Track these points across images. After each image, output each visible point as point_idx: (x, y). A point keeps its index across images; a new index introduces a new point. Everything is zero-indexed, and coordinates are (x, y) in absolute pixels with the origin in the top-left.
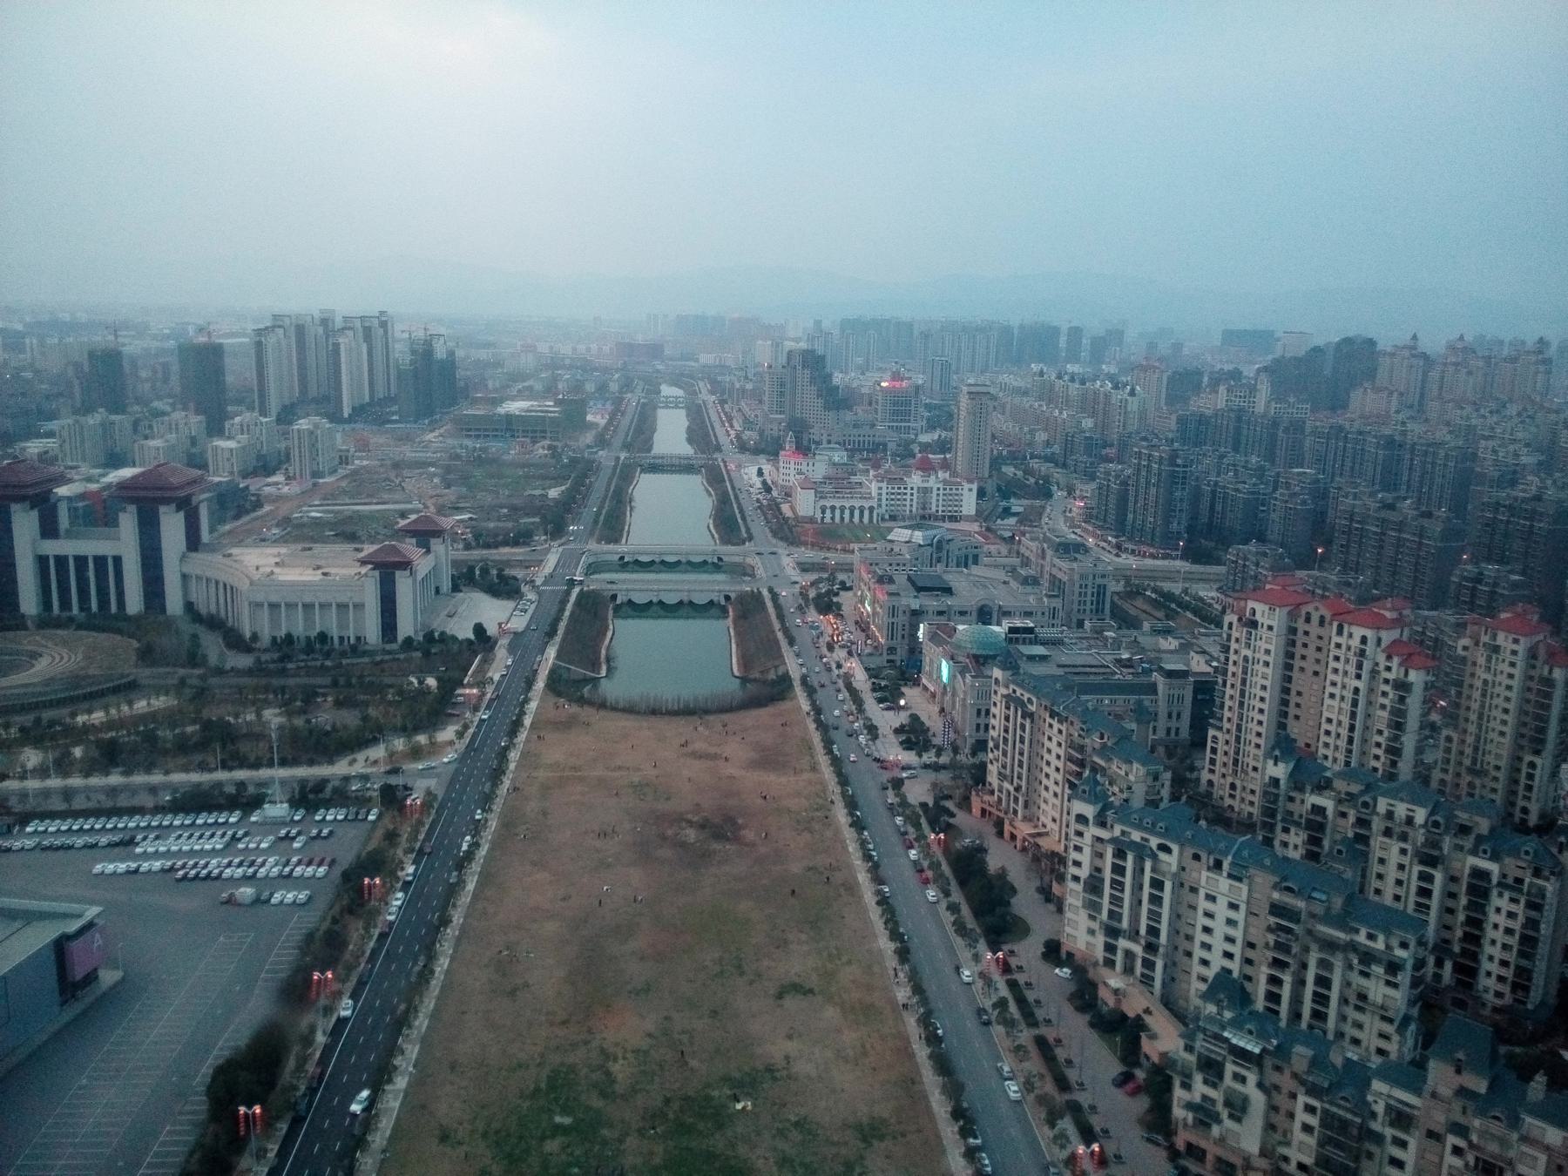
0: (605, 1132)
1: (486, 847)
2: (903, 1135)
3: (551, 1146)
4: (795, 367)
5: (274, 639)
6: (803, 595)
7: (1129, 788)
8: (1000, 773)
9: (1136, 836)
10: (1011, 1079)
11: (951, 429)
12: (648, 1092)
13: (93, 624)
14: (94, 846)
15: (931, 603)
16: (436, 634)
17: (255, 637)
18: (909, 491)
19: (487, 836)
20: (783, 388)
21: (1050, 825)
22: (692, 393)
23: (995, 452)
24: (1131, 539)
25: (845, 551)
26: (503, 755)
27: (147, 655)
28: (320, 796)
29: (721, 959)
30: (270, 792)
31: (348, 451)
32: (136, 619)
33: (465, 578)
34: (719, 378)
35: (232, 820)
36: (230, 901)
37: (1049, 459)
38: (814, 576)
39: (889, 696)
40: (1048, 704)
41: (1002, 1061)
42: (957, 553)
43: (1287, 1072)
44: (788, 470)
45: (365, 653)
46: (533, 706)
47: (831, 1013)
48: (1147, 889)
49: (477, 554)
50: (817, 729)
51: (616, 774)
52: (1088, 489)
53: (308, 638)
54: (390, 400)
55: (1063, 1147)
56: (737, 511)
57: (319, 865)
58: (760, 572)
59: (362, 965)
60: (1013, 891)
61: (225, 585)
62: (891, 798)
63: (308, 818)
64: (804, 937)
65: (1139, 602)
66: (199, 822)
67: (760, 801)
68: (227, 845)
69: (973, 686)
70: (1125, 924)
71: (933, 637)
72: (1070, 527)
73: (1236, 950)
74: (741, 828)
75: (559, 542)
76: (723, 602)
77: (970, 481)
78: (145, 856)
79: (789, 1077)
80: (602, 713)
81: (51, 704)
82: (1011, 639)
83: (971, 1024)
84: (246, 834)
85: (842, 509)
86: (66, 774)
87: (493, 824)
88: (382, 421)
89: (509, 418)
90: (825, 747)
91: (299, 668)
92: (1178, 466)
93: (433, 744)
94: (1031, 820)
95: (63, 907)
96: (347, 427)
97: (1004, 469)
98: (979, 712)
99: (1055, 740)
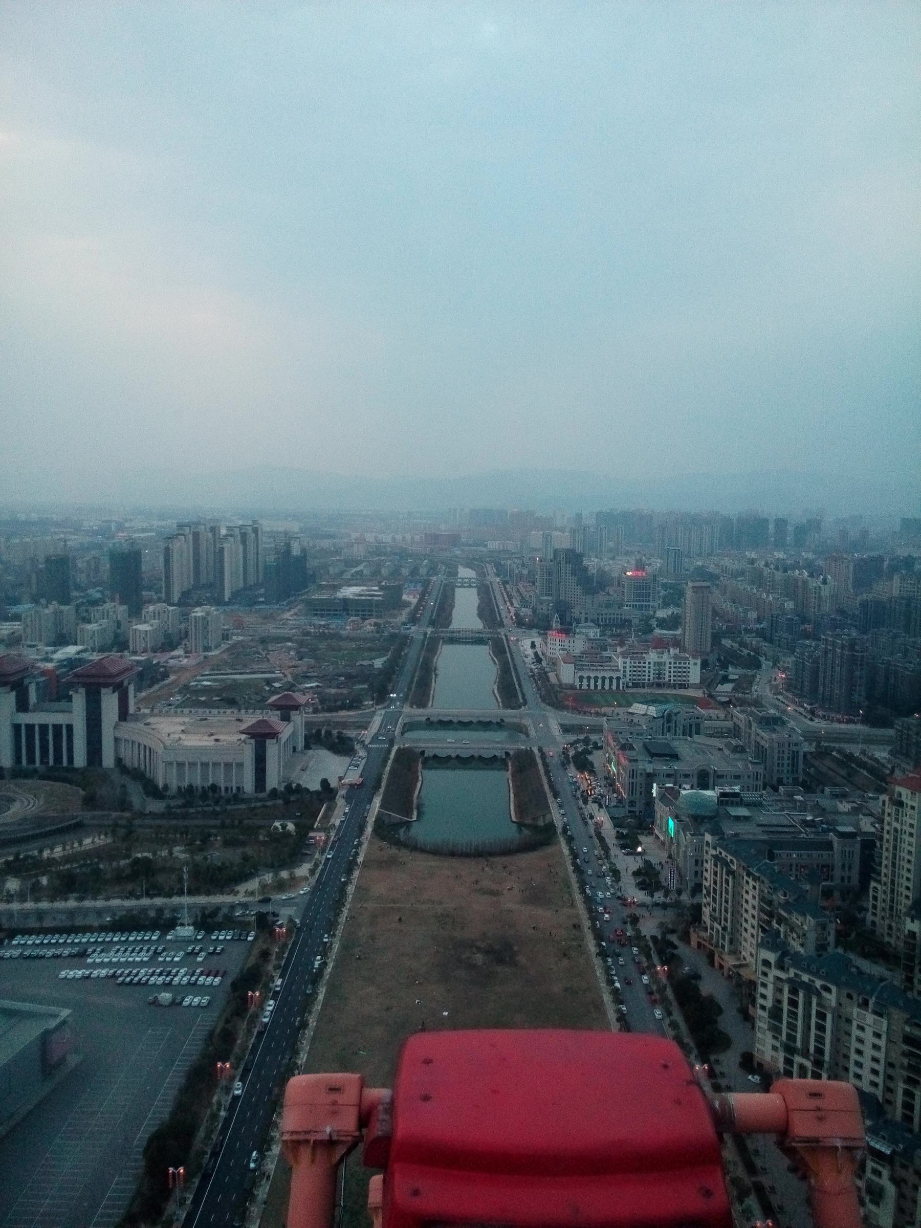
1: (331, 965)
5: (179, 788)
6: (565, 752)
7: (804, 935)
8: (711, 915)
9: (805, 978)
16: (294, 785)
17: (166, 787)
18: (647, 665)
21: (749, 959)
22: (482, 574)
24: (822, 707)
27: (90, 802)
32: (82, 772)
35: (154, 938)
36: (155, 1003)
37: (761, 634)
38: (572, 738)
40: (745, 865)
42: (683, 722)
43: (911, 1170)
45: (243, 801)
48: (814, 1020)
50: (574, 872)
51: (423, 907)
52: (789, 661)
53: (203, 788)
56: (515, 678)
57: (215, 976)
58: (532, 732)
60: (720, 1011)
61: (145, 747)
65: (828, 762)
67: (531, 931)
68: (151, 958)
70: (799, 1044)
71: (662, 797)
72: (775, 694)
73: (880, 1068)
77: (694, 657)
78: (95, 966)
80: (418, 855)
82: (722, 801)
84: (164, 950)
85: (596, 678)
86: (37, 900)
87: (336, 946)
88: (252, 603)
89: (345, 601)
92: (857, 651)
93: (293, 878)
95: (43, 1009)
96: (228, 608)
97: (724, 642)
98: (697, 862)
99: (751, 893)
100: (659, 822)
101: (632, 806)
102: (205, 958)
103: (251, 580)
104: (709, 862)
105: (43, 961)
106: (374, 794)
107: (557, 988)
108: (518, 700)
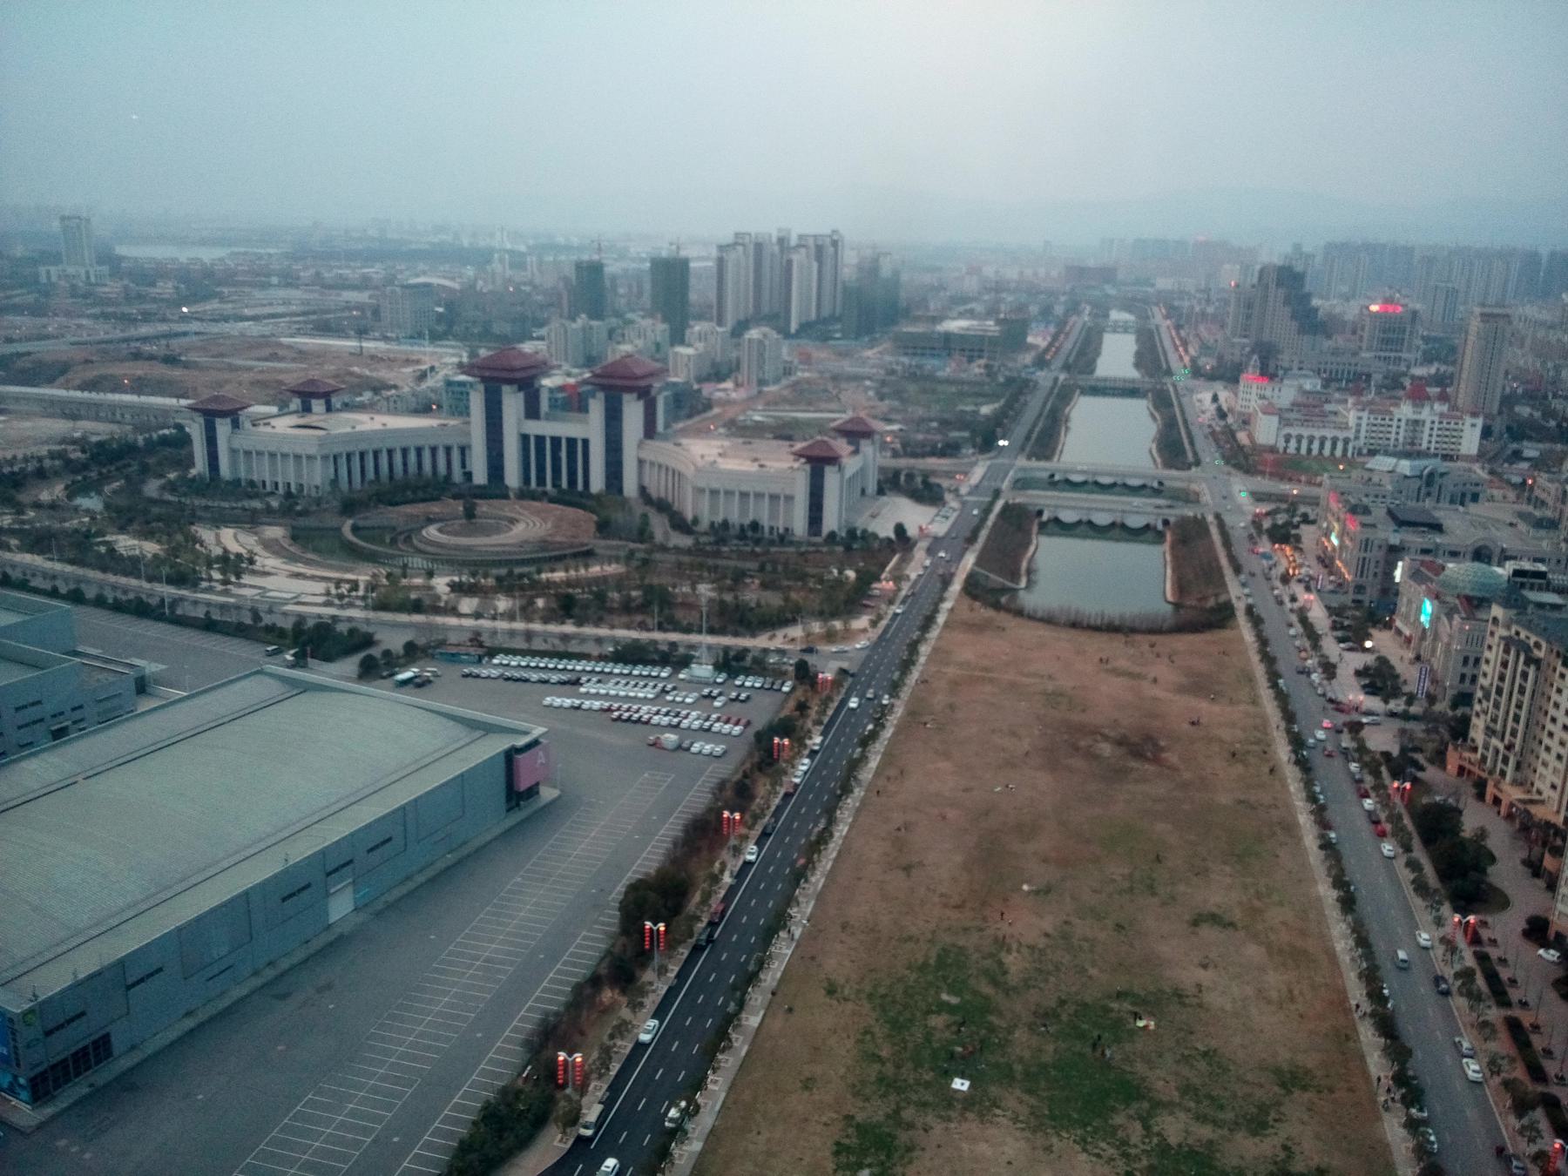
0: (993, 1019)
2: (1331, 1090)
3: (937, 1021)
4: (1267, 286)
5: (712, 524)
6: (1256, 522)
8: (1487, 728)
10: (1471, 1057)
11: (1454, 363)
12: (1040, 989)
13: (564, 498)
14: (546, 682)
15: (1415, 539)
16: (859, 532)
17: (696, 521)
19: (893, 720)
20: (1250, 304)
21: (1547, 792)
23: (1508, 390)
25: (1309, 483)
26: (913, 647)
27: (604, 528)
28: (742, 664)
29: (1131, 875)
30: (697, 654)
31: (791, 362)
32: (598, 497)
33: (891, 483)
34: (1176, 303)
39: (1353, 636)
41: (1461, 1035)
42: (1451, 488)
44: (1250, 395)
45: (791, 543)
46: (947, 605)
47: (1253, 951)
49: (903, 463)
50: (1261, 661)
51: (1032, 680)
53: (742, 526)
54: (834, 318)
55: (1531, 1140)
58: (1206, 498)
59: (767, 818)
62: (1346, 741)
63: (730, 682)
64: (1228, 869)
66: (636, 672)
67: (1186, 726)
68: (657, 696)
69: (1461, 630)
71: (1415, 575)
74: (1162, 749)
75: (988, 455)
76: (1160, 527)
77: (1474, 415)
78: (588, 695)
79: (1200, 1006)
80: (1019, 620)
81: (523, 562)
83: (1425, 989)
84: (674, 689)
85: (1311, 440)
86: (529, 619)
87: (899, 711)
88: (825, 338)
89: (948, 337)
90: (1269, 680)
91: (732, 551)
93: (847, 630)
94: (1521, 784)
98: (1466, 660)
100: (1403, 609)
101: (1359, 593)
102: (725, 705)
103: (826, 312)
104: (1494, 649)
105: (528, 684)
106: (967, 549)
107: (1224, 799)
108: (1186, 457)
